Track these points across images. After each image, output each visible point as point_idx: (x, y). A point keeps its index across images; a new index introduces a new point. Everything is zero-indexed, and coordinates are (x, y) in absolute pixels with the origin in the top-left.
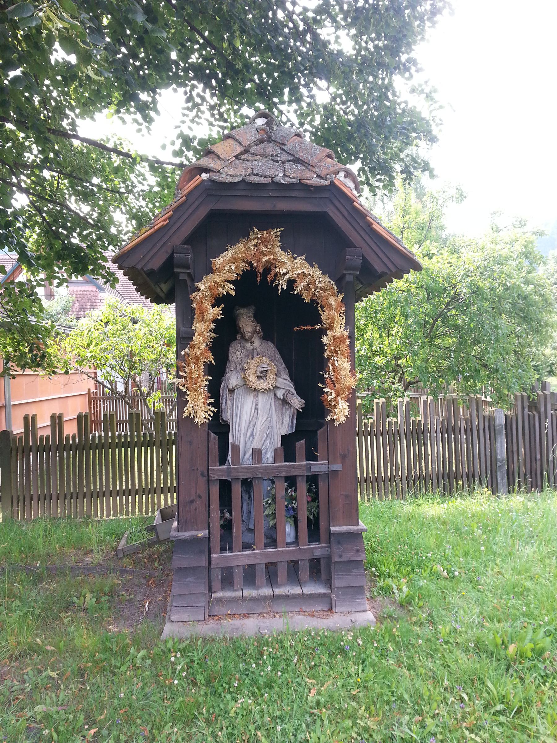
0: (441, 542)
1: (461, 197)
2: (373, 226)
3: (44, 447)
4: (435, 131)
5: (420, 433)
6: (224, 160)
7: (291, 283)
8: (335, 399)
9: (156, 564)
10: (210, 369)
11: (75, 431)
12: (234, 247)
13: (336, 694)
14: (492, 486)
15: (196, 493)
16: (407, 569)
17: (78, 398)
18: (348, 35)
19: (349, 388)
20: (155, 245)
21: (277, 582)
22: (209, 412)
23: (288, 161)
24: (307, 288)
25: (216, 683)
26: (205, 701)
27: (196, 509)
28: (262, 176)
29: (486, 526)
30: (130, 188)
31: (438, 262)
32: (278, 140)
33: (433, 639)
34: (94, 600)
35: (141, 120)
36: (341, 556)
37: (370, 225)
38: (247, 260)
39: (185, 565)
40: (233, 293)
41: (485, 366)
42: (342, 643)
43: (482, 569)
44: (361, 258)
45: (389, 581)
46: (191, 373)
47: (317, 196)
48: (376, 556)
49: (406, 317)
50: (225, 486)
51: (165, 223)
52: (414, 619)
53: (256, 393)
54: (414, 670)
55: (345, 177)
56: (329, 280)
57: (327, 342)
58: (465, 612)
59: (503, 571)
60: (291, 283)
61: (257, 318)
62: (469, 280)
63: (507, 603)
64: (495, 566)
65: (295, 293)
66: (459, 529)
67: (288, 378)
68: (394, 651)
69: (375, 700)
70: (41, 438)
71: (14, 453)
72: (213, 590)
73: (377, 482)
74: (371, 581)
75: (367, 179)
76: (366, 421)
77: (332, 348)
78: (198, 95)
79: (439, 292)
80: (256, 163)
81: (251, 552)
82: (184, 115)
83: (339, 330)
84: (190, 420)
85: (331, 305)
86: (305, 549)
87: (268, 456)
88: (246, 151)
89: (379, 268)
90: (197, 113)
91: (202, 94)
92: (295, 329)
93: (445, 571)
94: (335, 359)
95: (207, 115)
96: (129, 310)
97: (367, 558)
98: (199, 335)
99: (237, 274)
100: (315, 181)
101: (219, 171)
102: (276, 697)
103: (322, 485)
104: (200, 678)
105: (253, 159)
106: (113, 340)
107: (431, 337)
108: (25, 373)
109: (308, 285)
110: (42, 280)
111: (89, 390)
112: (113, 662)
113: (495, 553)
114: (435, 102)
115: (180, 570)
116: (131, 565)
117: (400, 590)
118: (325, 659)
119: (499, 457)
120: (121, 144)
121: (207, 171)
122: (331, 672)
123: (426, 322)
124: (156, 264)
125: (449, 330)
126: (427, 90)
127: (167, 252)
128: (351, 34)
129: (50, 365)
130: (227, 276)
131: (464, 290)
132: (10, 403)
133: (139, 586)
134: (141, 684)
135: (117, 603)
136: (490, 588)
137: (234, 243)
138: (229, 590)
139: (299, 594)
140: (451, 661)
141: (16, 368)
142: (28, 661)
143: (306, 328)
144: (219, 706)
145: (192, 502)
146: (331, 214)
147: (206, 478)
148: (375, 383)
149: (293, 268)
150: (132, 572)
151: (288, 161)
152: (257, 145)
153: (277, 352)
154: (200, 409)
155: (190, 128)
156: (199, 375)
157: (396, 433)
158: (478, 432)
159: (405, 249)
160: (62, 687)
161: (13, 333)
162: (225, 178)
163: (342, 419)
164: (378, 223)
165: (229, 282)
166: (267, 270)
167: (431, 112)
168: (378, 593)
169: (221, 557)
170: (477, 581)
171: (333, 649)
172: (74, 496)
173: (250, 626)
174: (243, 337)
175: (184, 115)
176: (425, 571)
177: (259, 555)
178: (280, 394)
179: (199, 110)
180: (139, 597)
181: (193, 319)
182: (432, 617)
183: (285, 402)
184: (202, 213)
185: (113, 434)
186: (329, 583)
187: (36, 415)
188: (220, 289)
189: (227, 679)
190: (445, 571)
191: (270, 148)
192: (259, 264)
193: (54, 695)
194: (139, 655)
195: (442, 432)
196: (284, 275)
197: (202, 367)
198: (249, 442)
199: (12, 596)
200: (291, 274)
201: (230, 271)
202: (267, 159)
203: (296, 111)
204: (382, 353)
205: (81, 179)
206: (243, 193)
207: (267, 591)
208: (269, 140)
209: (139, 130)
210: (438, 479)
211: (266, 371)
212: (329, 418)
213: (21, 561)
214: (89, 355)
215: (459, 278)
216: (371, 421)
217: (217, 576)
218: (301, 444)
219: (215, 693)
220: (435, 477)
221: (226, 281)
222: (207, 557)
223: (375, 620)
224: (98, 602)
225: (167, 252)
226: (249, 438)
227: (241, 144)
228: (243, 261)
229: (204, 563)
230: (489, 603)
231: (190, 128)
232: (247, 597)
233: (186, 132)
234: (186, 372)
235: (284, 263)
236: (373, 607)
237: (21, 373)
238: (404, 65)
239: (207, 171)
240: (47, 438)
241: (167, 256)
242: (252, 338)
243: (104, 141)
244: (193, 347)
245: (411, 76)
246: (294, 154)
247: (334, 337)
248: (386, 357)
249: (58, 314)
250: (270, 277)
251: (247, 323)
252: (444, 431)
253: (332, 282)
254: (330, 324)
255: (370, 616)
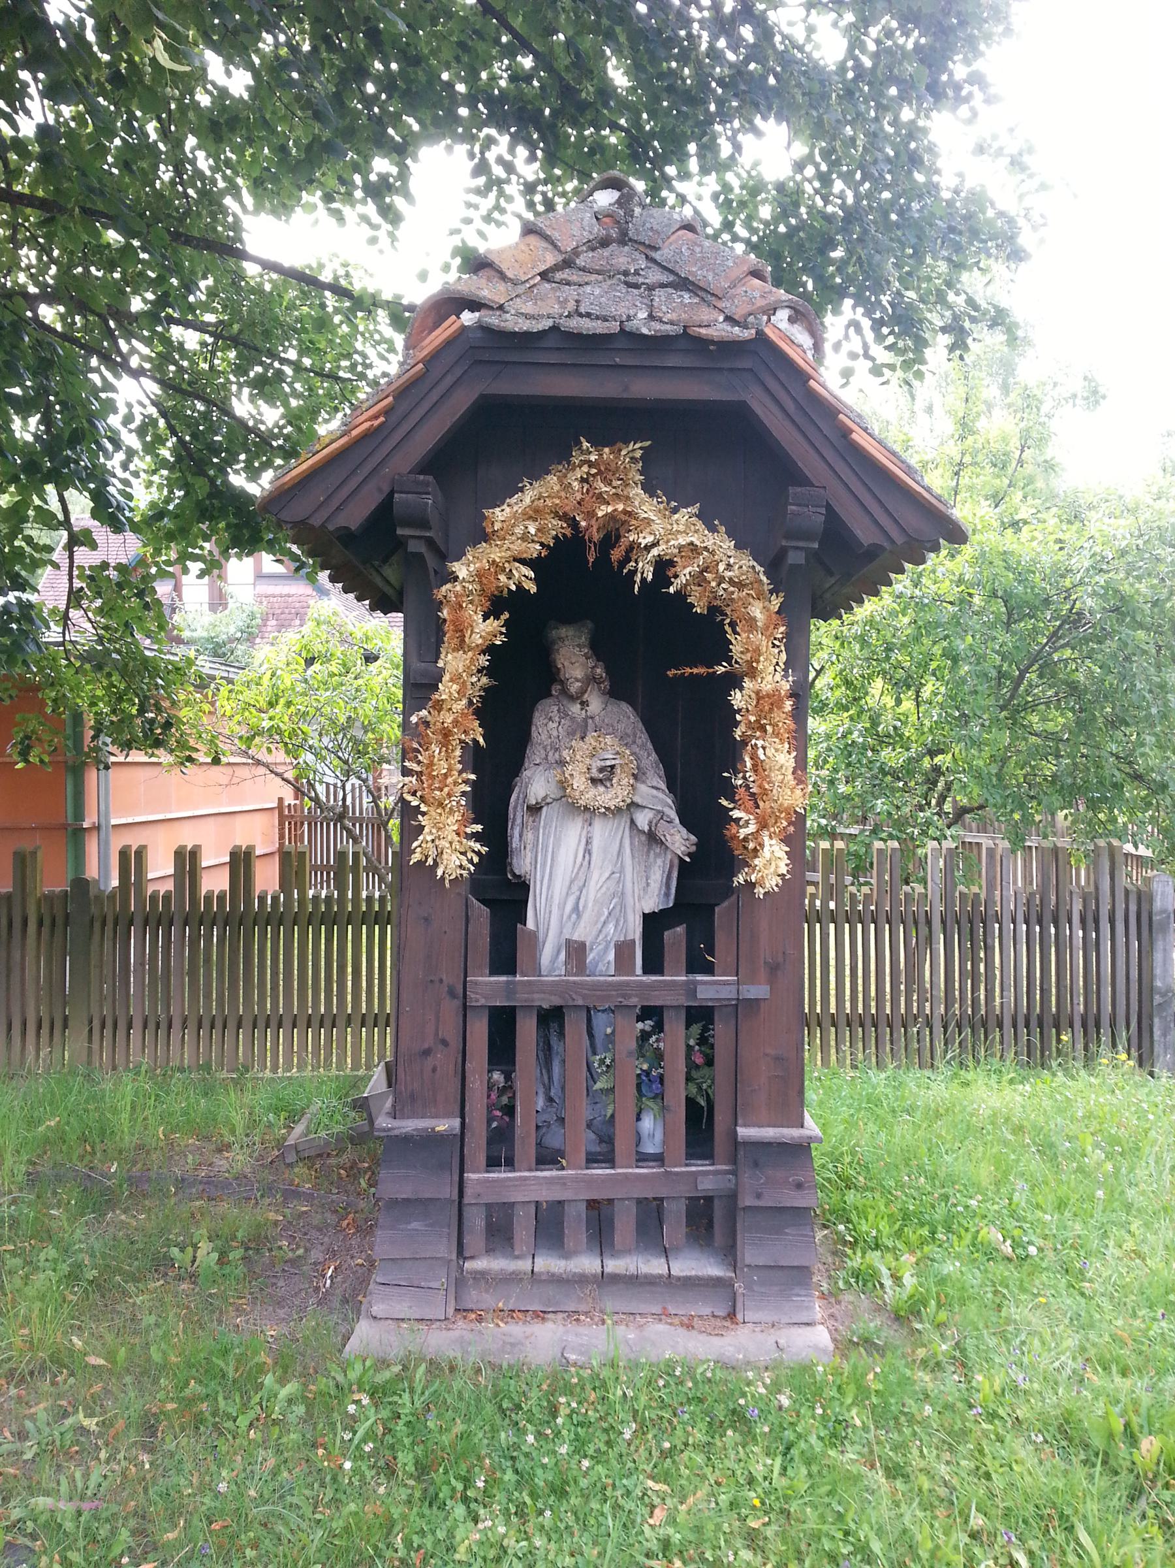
0: (1006, 1174)
1: (1094, 396)
2: (854, 436)
3: (159, 917)
4: (1025, 240)
5: (977, 920)
6: (515, 283)
7: (663, 566)
8: (756, 835)
9: (363, 1184)
10: (475, 757)
11: (226, 886)
12: (536, 484)
13: (710, 1526)
14: (1140, 1047)
15: (437, 1034)
16: (920, 1232)
17: (258, 815)
18: (835, 25)
19: (788, 811)
20: (353, 472)
21: (612, 1245)
22: (470, 854)
23: (663, 286)
24: (699, 579)
25: (438, 1476)
26: (404, 1517)
27: (434, 1070)
28: (597, 318)
29: (1114, 1141)
30: (360, 368)
31: (1033, 539)
32: (641, 238)
33: (959, 1405)
34: (215, 1256)
35: (376, 219)
36: (759, 1196)
37: (846, 433)
38: (565, 514)
39: (405, 1191)
40: (533, 588)
41: (1137, 777)
42: (742, 1401)
43: (1095, 1244)
44: (823, 511)
45: (874, 1257)
46: (431, 764)
47: (726, 365)
48: (851, 1197)
49: (955, 660)
50: (503, 1022)
51: (376, 423)
52: (921, 1353)
53: (587, 815)
54: (906, 1477)
55: (791, 320)
56: (753, 563)
57: (742, 705)
58: (1043, 1343)
59: (1145, 1249)
60: (663, 566)
61: (598, 649)
62: (1101, 579)
63: (1149, 1329)
64: (1127, 1237)
65: (672, 590)
66: (1052, 1145)
67: (663, 786)
68: (865, 1428)
69: (803, 1547)
70: (154, 897)
71: (97, 926)
72: (467, 1254)
73: (875, 1025)
74: (835, 1253)
75: (866, 347)
76: (853, 889)
77: (753, 719)
78: (500, 160)
79: (1034, 608)
80: (588, 289)
81: (555, 1173)
82: (469, 205)
83: (772, 678)
84: (426, 870)
85: (754, 619)
86: (677, 1174)
87: (602, 960)
88: (567, 264)
89: (865, 534)
90: (498, 200)
91: (508, 157)
92: (670, 673)
93: (1009, 1242)
94: (760, 743)
95: (519, 205)
96: (359, 634)
97: (823, 1200)
98: (451, 680)
99: (542, 544)
100: (720, 330)
101: (501, 307)
102: (570, 1519)
103: (721, 1031)
104: (406, 1459)
105: (580, 280)
106: (324, 695)
107: (1014, 711)
108: (129, 759)
109: (701, 572)
110: (168, 563)
111: (281, 800)
112: (222, 1403)
113: (1128, 1207)
114: (1031, 176)
115: (394, 1203)
116: (309, 1181)
117: (897, 1279)
118: (699, 1435)
119: (1158, 983)
120: (347, 275)
121: (475, 305)
122: (708, 1471)
123: (1001, 675)
124: (354, 517)
125: (1057, 694)
126: (1012, 148)
127: (380, 490)
128: (842, 24)
129: (182, 745)
130: (518, 547)
131: (1089, 602)
132: (107, 821)
133: (320, 1230)
134: (271, 1462)
135: (259, 1264)
136: (1110, 1288)
137: (536, 475)
138: (505, 1256)
139: (661, 1276)
140: (997, 1463)
141: (111, 748)
142: (45, 1386)
143: (695, 671)
144: (433, 1533)
145: (427, 1053)
146: (759, 410)
147: (458, 1003)
148: (880, 804)
149: (670, 534)
150: (309, 1198)
151: (663, 286)
152: (593, 249)
153: (640, 725)
154: (450, 846)
155: (481, 234)
156: (450, 769)
157: (922, 919)
158: (1112, 921)
159: (928, 490)
160: (103, 1455)
161: (109, 675)
162: (512, 323)
163: (772, 883)
164: (865, 430)
165: (523, 562)
166: (611, 538)
167: (1021, 197)
168: (847, 1282)
169: (487, 1180)
170: (1081, 1272)
171: (720, 1412)
172: (219, 1024)
173: (544, 1341)
174: (565, 692)
175: (469, 205)
176: (960, 1237)
177: (570, 1182)
178: (643, 819)
179: (501, 192)
180: (316, 1255)
181: (439, 642)
182: (963, 1351)
183: (653, 838)
184: (462, 401)
185: (303, 893)
186: (730, 1253)
187: (145, 847)
188: (503, 578)
189: (464, 1467)
190: (1009, 1242)
191: (622, 258)
192: (593, 522)
193: (78, 1475)
194: (284, 1393)
195: (1027, 922)
196: (648, 548)
197: (458, 753)
198: (570, 924)
199: (45, 1235)
200: (663, 547)
201: (525, 537)
202: (614, 281)
203: (715, 197)
204: (895, 738)
205: (256, 349)
206: (553, 358)
207: (588, 1264)
208: (624, 239)
209: (373, 241)
210: (1015, 1026)
211: (612, 767)
212: (741, 879)
213: (81, 1158)
214: (266, 724)
215: (1079, 576)
216: (865, 890)
217: (476, 1221)
218: (675, 936)
219: (432, 1500)
220: (1007, 1022)
221: (515, 560)
222: (456, 1178)
223: (831, 1346)
224: (222, 1261)
225: (380, 490)
226: (570, 917)
227: (555, 246)
228: (556, 515)
229: (448, 1191)
230: (1105, 1325)
231: (481, 234)
232: (541, 1273)
233: (475, 242)
234: (419, 762)
235: (648, 522)
236: (832, 1316)
237: (121, 759)
238: (958, 88)
239: (475, 305)
240: (167, 897)
241: (378, 498)
242: (583, 692)
243: (311, 268)
244: (439, 706)
245: (975, 113)
246: (677, 269)
247: (757, 693)
248: (908, 749)
249: (231, 641)
250: (616, 554)
251: (574, 660)
252: (1033, 919)
253: (758, 568)
254: (749, 663)
255: (821, 1336)
